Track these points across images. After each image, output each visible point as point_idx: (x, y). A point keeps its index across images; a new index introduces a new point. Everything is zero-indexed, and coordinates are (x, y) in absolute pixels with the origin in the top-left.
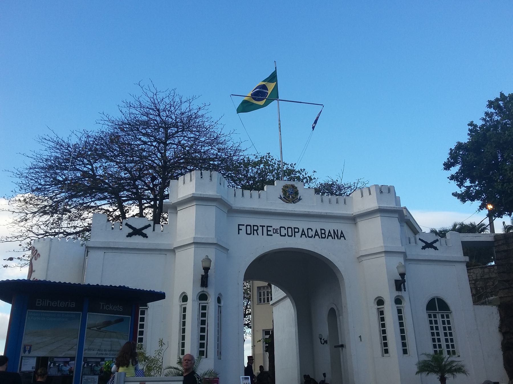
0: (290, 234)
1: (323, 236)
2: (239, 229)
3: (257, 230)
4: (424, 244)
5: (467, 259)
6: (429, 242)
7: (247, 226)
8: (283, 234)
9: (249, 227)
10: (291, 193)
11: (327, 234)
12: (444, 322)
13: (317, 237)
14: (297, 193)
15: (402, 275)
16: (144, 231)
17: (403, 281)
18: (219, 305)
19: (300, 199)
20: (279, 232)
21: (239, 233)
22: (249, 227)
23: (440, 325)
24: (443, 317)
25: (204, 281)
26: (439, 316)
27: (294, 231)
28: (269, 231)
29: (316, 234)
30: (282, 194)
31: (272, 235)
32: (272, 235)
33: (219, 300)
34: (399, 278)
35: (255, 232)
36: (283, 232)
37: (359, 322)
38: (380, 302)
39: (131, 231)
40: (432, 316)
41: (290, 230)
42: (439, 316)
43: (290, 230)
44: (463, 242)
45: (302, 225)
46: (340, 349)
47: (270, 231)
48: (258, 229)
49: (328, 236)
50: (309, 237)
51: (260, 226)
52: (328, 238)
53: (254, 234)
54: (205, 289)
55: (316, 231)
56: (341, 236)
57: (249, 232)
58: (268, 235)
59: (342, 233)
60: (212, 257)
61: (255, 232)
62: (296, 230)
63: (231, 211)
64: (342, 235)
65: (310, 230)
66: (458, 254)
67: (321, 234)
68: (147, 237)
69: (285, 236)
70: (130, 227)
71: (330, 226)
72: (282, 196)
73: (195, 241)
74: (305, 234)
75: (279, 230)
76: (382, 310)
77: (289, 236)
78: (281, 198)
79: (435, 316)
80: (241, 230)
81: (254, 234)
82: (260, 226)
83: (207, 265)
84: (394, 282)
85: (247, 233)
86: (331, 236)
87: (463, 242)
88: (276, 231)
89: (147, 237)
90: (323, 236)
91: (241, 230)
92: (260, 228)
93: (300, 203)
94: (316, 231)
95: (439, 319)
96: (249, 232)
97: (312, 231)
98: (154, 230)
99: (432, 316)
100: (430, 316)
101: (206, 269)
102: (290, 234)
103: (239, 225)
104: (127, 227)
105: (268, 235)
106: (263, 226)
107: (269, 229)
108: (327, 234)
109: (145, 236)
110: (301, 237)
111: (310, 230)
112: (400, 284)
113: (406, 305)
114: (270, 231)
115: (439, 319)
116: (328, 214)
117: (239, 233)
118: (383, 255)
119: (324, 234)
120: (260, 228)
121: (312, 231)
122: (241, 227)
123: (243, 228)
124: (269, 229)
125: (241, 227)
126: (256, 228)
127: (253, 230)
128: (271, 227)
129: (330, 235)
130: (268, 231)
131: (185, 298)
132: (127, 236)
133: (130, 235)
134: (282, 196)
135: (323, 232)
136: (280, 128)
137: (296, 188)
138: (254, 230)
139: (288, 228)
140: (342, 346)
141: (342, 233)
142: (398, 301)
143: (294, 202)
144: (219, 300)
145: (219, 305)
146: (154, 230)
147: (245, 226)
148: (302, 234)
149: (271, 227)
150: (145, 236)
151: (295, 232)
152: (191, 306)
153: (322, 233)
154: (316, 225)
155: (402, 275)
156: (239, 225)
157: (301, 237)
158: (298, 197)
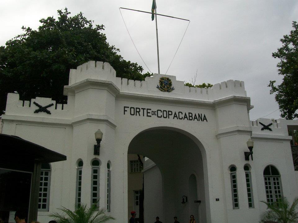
0: (165, 116)
1: (191, 118)
2: (125, 111)
3: (139, 112)
4: (263, 127)
5: (291, 138)
6: (266, 125)
7: (131, 108)
8: (181, 117)
9: (132, 110)
10: (166, 83)
11: (193, 117)
12: (275, 183)
13: (186, 119)
14: (170, 84)
15: (251, 148)
16: (48, 109)
17: (251, 153)
18: (109, 170)
19: (173, 89)
20: (156, 114)
21: (124, 114)
22: (132, 110)
23: (272, 185)
24: (274, 179)
25: (97, 150)
26: (272, 179)
27: (169, 113)
28: (149, 113)
29: (186, 116)
30: (159, 84)
31: (151, 116)
32: (151, 116)
33: (108, 166)
34: (249, 151)
35: (138, 113)
36: (160, 114)
37: (216, 183)
38: (233, 169)
39: (37, 108)
40: (267, 179)
41: (165, 112)
42: (272, 179)
43: (165, 112)
44: (288, 126)
45: (175, 109)
46: (198, 203)
47: (150, 113)
48: (140, 111)
49: (195, 118)
50: (180, 119)
51: (142, 109)
52: (194, 120)
53: (136, 115)
54: (97, 157)
55: (185, 115)
56: (204, 119)
57: (132, 113)
58: (147, 116)
59: (205, 116)
60: (104, 132)
61: (138, 113)
62: (170, 113)
63: (119, 96)
64: (205, 118)
65: (180, 114)
66: (283, 134)
67: (189, 117)
68: (50, 114)
69: (161, 117)
70: (37, 105)
71: (195, 111)
72: (159, 86)
73: (254, 123)
74: (176, 116)
75: (156, 113)
76: (234, 174)
77: (164, 117)
78: (158, 87)
79: (269, 179)
80: (126, 111)
81: (136, 115)
82: (142, 109)
83: (99, 137)
84: (244, 153)
85: (131, 114)
86: (197, 118)
87: (288, 126)
88: (154, 113)
89: (50, 114)
90: (191, 118)
91: (126, 111)
92: (142, 111)
93: (173, 92)
94: (185, 115)
95: (272, 181)
96: (132, 113)
97: (182, 114)
98: (56, 108)
99: (267, 179)
100: (265, 179)
101: (99, 141)
102: (165, 116)
103: (125, 107)
104: (35, 105)
105: (147, 116)
106: (144, 109)
107: (149, 111)
108: (193, 117)
109: (49, 113)
110: (174, 118)
111: (180, 114)
112: (248, 155)
113: (252, 171)
114: (150, 113)
115: (272, 181)
116: (205, 102)
117: (124, 114)
118: (237, 133)
119: (192, 116)
120: (142, 111)
121: (182, 114)
122: (126, 109)
123: (128, 110)
124: (149, 111)
125: (126, 109)
126: (138, 110)
127: (136, 111)
128: (150, 109)
129: (196, 118)
130: (148, 113)
131: (80, 163)
132: (35, 112)
133: (37, 112)
134: (159, 86)
135: (191, 115)
136: (157, 30)
137: (170, 80)
138: (137, 112)
139: (164, 111)
140: (200, 202)
141: (205, 116)
142: (247, 168)
143: (168, 91)
144: (108, 166)
145: (109, 170)
146: (56, 108)
147: (129, 109)
148: (174, 117)
149: (150, 109)
150: (49, 113)
151: (169, 115)
152: (87, 170)
153: (189, 116)
154: (186, 110)
155: (251, 148)
156: (125, 107)
157: (174, 118)
158: (172, 87)
